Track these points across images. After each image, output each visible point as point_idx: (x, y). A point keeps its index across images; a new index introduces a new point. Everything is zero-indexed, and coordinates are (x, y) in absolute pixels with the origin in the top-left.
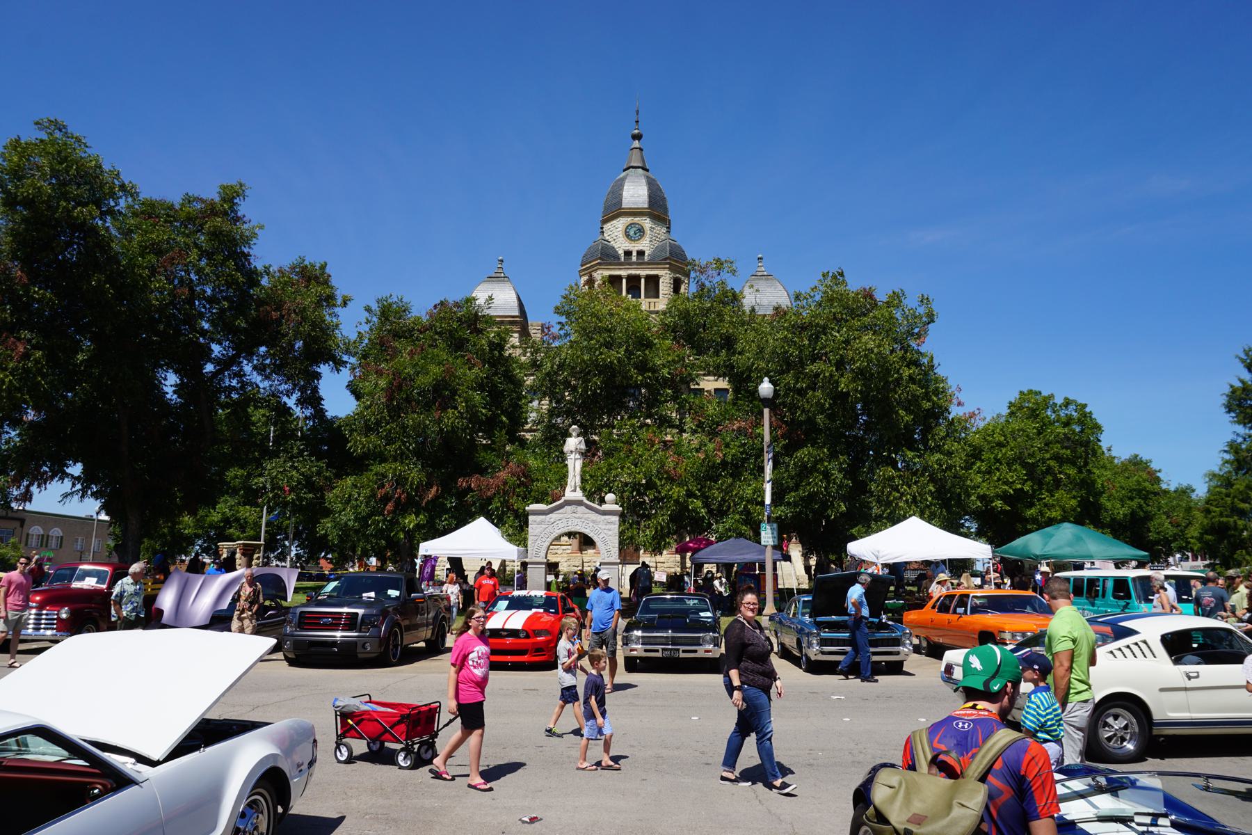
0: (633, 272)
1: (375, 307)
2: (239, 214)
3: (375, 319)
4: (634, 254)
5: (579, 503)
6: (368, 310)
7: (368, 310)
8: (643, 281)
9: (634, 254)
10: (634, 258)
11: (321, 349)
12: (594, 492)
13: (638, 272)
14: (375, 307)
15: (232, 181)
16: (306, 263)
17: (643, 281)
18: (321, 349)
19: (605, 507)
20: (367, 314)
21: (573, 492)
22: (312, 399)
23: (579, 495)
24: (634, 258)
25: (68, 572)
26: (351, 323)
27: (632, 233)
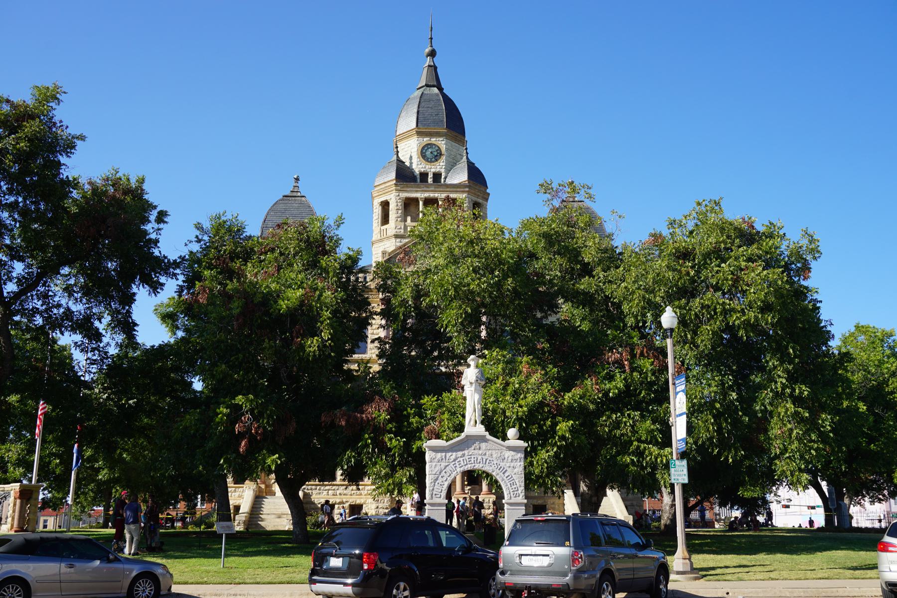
0: (432, 195)
1: (207, 225)
2: (56, 119)
3: (206, 238)
4: (430, 176)
5: (482, 439)
6: (199, 227)
7: (199, 227)
8: (421, 203)
9: (430, 176)
10: (430, 180)
11: (148, 267)
12: (494, 426)
13: (436, 195)
14: (207, 225)
15: (48, 83)
16: (119, 175)
17: (421, 203)
18: (148, 267)
19: (507, 443)
20: (198, 233)
21: (473, 427)
22: (127, 326)
23: (480, 429)
24: (430, 180)
25: (315, 578)
26: (174, 241)
27: (428, 153)
